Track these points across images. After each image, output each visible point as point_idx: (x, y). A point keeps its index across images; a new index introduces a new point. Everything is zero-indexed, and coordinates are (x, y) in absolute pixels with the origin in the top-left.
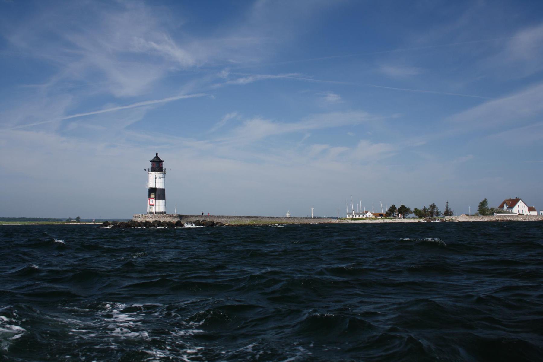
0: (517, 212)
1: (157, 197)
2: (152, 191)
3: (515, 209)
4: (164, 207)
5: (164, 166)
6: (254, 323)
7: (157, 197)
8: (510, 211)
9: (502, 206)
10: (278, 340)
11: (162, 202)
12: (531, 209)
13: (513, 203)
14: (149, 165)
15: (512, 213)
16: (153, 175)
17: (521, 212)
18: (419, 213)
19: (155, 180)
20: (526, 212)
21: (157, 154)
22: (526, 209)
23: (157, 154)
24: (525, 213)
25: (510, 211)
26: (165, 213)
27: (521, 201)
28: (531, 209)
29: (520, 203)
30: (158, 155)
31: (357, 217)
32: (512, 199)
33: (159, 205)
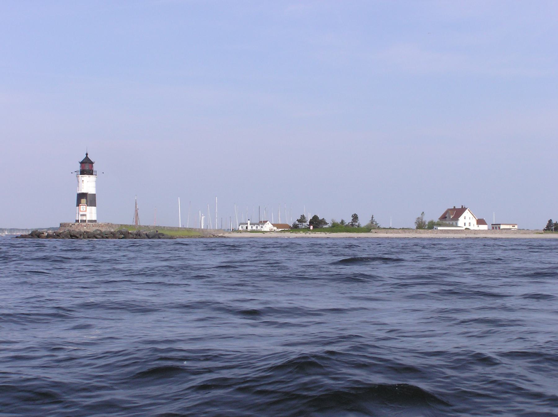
0: (462, 225)
1: (88, 203)
2: (82, 196)
3: (461, 221)
4: (96, 215)
5: (459, 207)
6: (165, 319)
7: (88, 203)
8: (454, 223)
9: (444, 217)
10: (436, 315)
11: (94, 208)
12: (480, 222)
13: (459, 212)
14: (78, 167)
15: (457, 226)
16: (86, 178)
17: (467, 226)
18: (336, 227)
19: (88, 185)
20: (474, 226)
21: (87, 154)
22: (474, 222)
23: (87, 154)
24: (472, 228)
25: (454, 224)
26: (95, 221)
27: (467, 211)
28: (480, 222)
29: (467, 214)
30: (88, 156)
31: (254, 228)
32: (456, 208)
33: (91, 213)
